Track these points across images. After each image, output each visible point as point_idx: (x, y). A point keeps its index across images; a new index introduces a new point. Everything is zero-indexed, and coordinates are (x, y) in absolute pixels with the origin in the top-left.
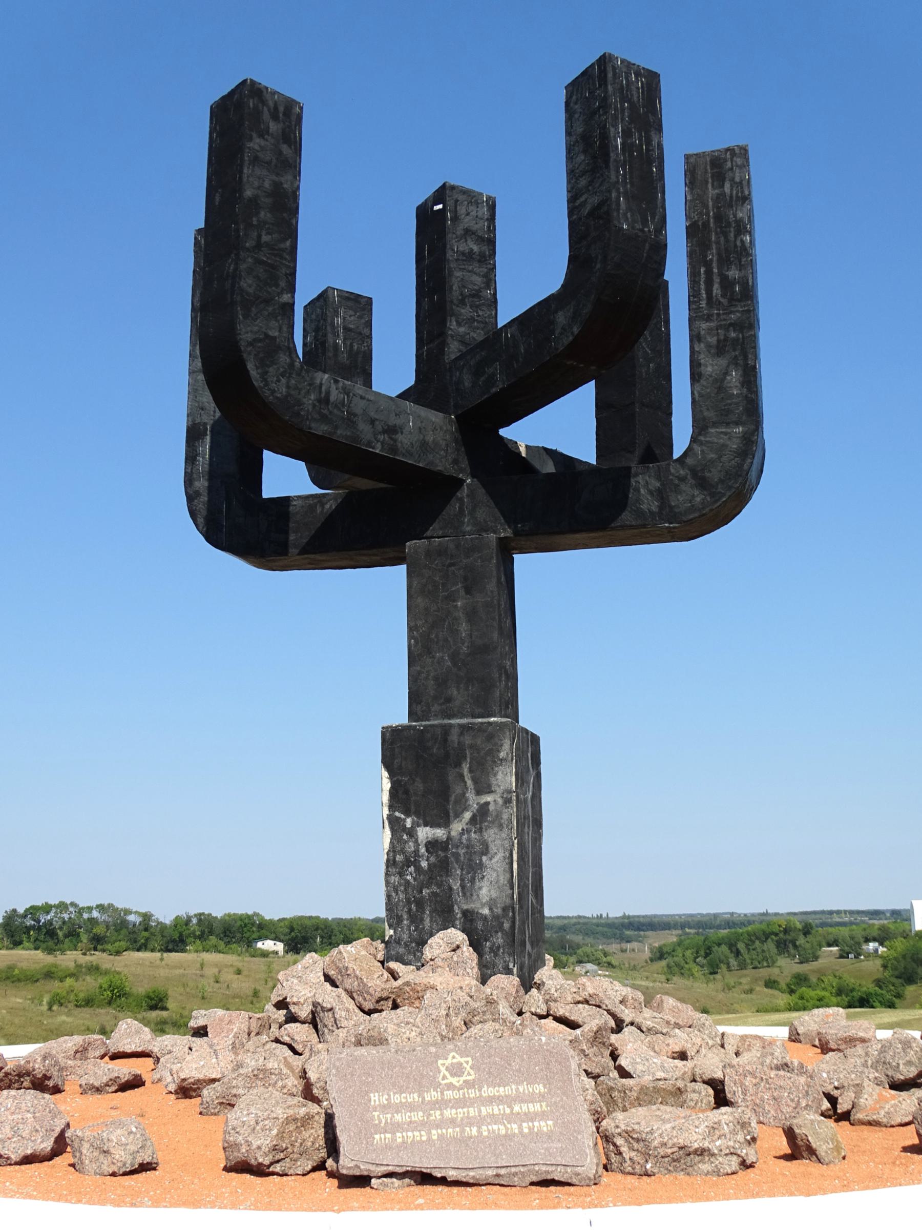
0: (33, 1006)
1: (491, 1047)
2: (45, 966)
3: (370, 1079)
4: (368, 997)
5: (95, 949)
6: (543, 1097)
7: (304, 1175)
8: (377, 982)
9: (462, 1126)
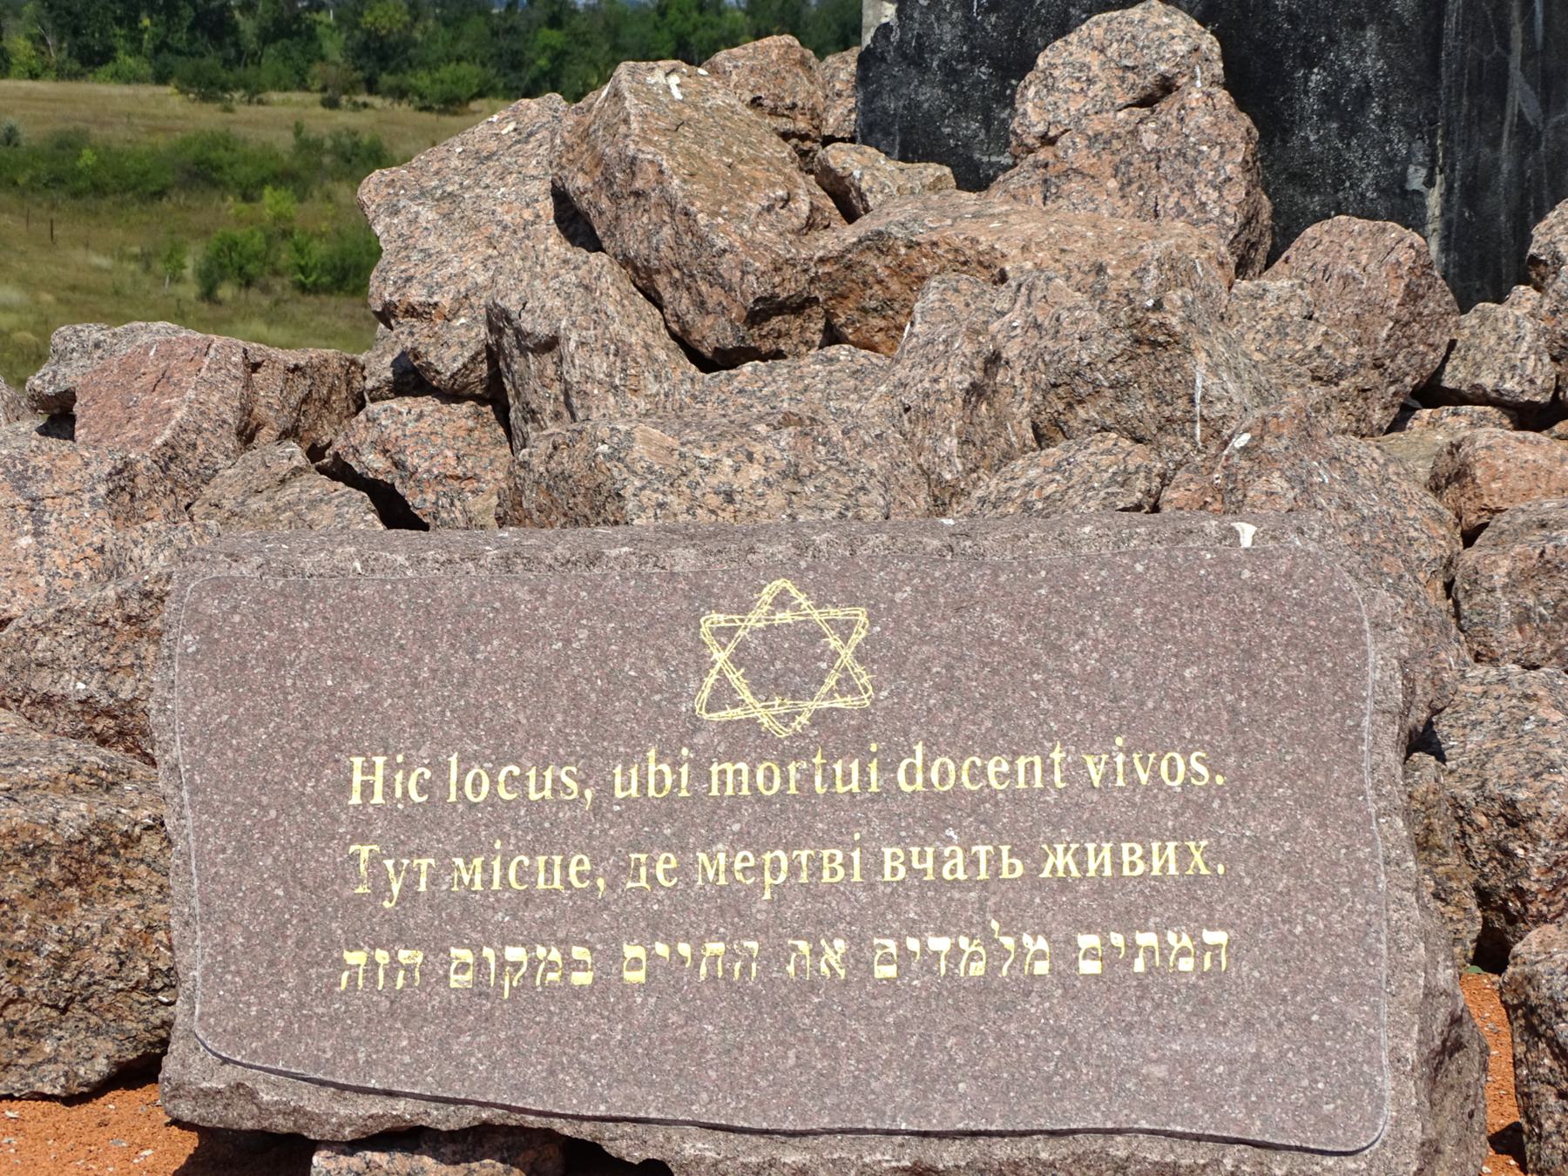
0: (147, 282)
1: (977, 559)
2: (187, 143)
3: (358, 688)
4: (714, 296)
5: (371, 87)
6: (1202, 810)
7: (70, 1100)
8: (757, 228)
9: (776, 932)
